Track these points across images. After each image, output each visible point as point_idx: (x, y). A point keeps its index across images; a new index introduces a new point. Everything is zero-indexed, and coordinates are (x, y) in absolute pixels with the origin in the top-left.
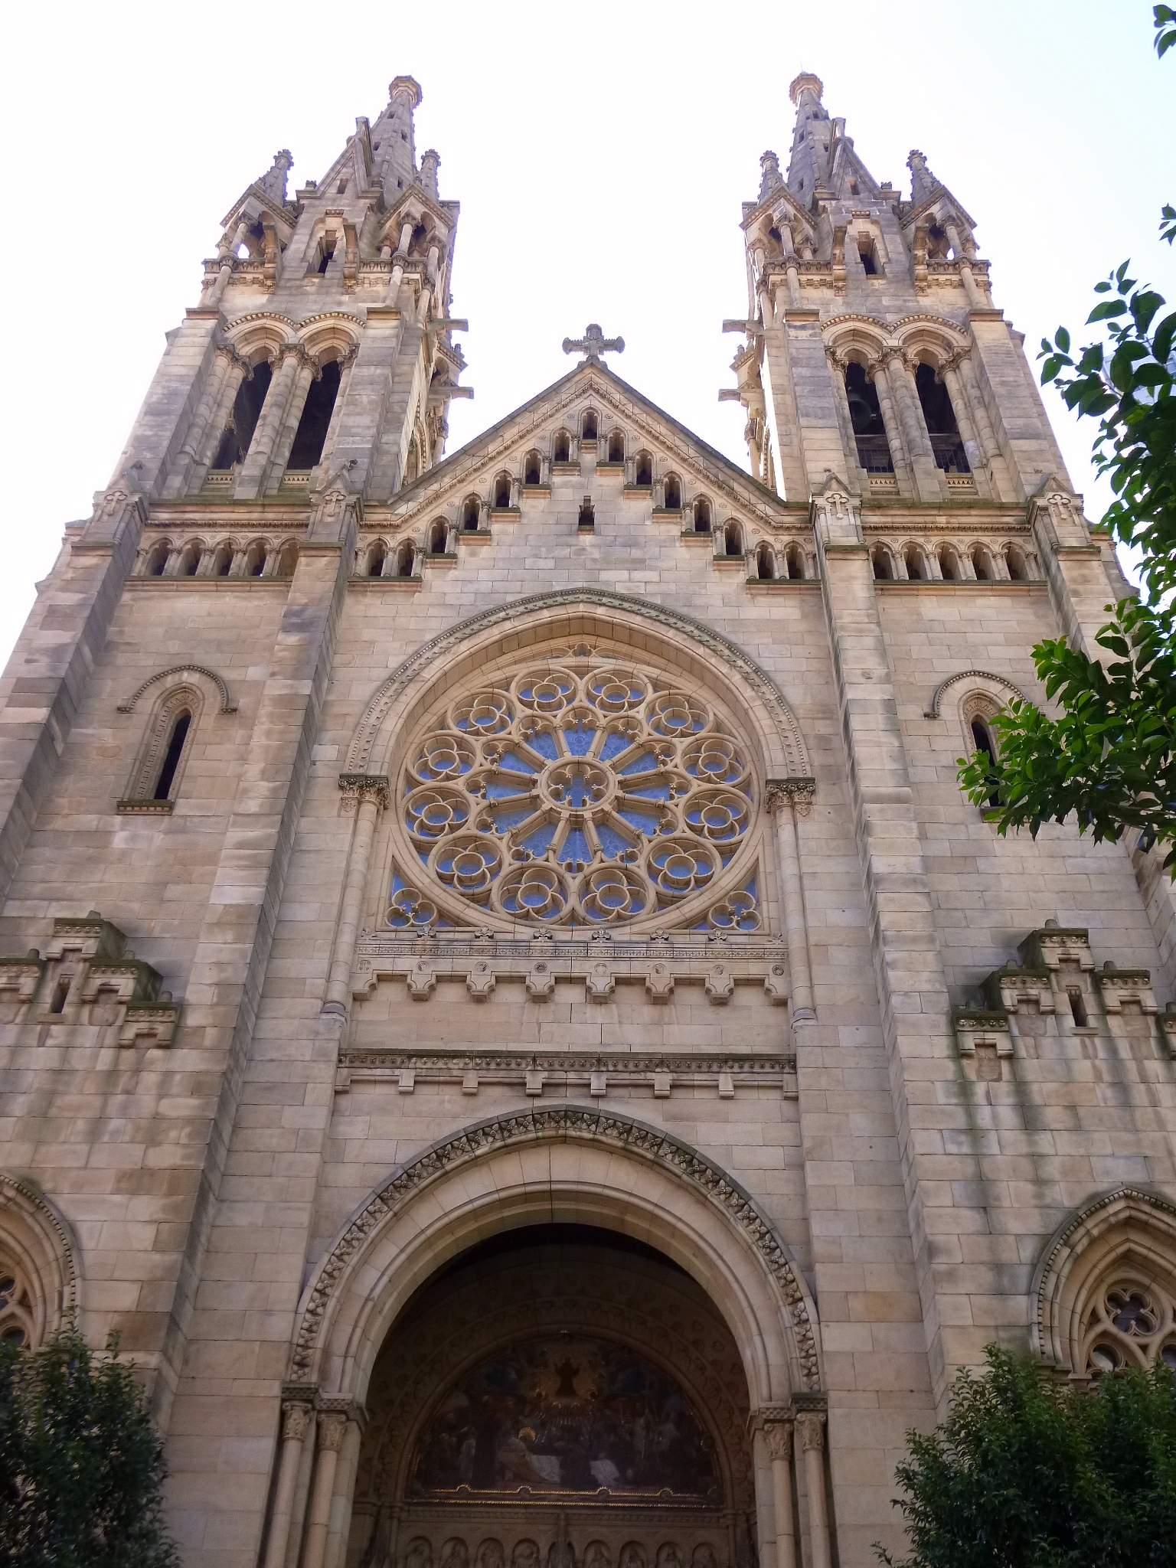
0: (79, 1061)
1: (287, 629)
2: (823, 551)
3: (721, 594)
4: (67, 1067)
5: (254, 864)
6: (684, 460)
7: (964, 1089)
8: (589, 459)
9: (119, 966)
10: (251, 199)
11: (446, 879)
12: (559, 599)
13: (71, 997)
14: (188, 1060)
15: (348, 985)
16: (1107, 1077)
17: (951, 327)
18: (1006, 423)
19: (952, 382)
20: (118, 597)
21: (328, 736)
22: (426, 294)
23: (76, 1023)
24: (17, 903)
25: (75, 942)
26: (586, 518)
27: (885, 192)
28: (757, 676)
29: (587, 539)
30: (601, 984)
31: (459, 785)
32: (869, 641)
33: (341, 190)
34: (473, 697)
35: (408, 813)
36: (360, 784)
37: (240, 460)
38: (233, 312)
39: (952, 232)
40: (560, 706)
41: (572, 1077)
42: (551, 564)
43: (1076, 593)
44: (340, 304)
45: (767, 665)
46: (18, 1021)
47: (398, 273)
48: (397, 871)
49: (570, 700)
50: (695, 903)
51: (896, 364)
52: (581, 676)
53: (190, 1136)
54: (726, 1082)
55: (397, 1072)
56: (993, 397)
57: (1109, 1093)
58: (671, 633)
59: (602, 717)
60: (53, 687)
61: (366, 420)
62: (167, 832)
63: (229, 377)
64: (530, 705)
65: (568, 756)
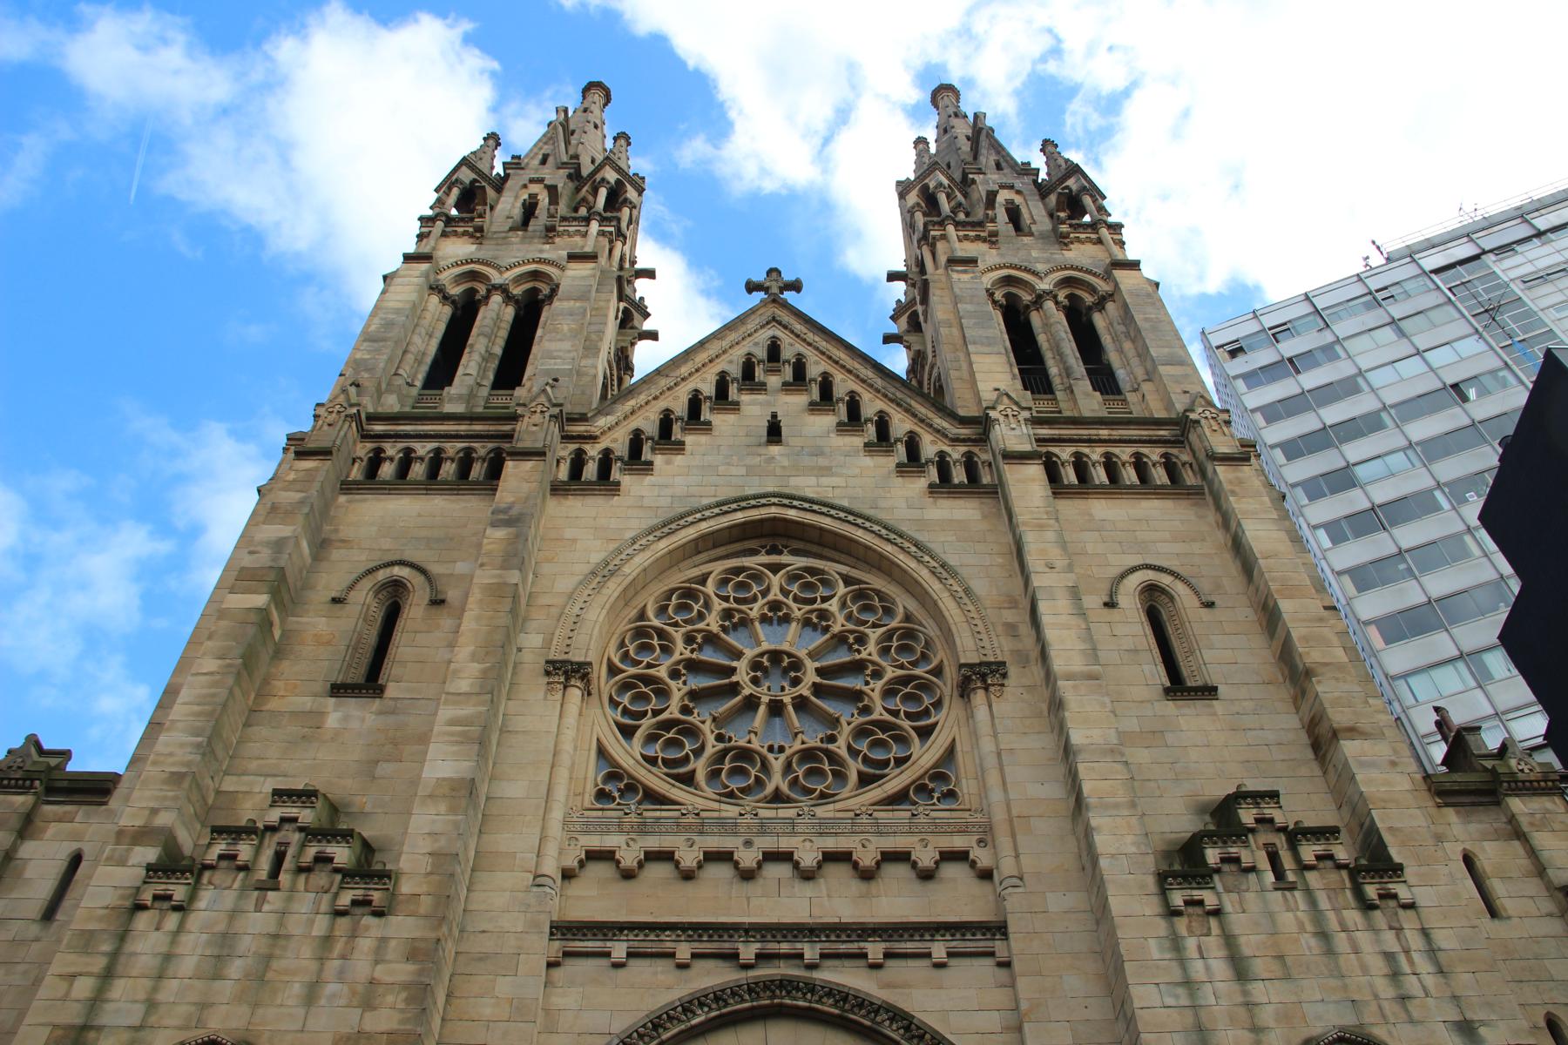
0: (295, 926)
1: (494, 525)
2: (999, 458)
3: (903, 500)
4: (283, 932)
5: (465, 739)
6: (863, 381)
7: (1176, 944)
8: (774, 381)
9: (334, 836)
10: (464, 168)
11: (652, 761)
12: (753, 502)
13: (288, 863)
14: (401, 927)
15: (558, 860)
16: (1309, 927)
17: (1094, 274)
18: (1153, 352)
19: (1099, 320)
20: (334, 499)
21: (532, 625)
22: (619, 244)
23: (293, 889)
24: (234, 778)
25: (292, 811)
26: (774, 432)
27: (1026, 170)
28: (944, 570)
29: (775, 450)
30: (808, 858)
31: (662, 672)
32: (1050, 535)
33: (544, 161)
34: (672, 591)
35: (611, 699)
36: (567, 672)
37: (450, 384)
38: (444, 258)
39: (1087, 200)
40: (755, 599)
41: (785, 947)
42: (743, 471)
43: (1233, 493)
44: (541, 251)
45: (952, 561)
46: (236, 886)
47: (594, 226)
48: (602, 752)
49: (765, 593)
50: (896, 781)
51: (1049, 305)
52: (775, 572)
53: (407, 1000)
54: (939, 950)
55: (609, 944)
56: (1138, 331)
57: (1313, 942)
58: (860, 533)
59: (797, 611)
60: (272, 576)
61: (567, 345)
62: (380, 713)
63: (438, 315)
64: (726, 599)
65: (765, 646)
